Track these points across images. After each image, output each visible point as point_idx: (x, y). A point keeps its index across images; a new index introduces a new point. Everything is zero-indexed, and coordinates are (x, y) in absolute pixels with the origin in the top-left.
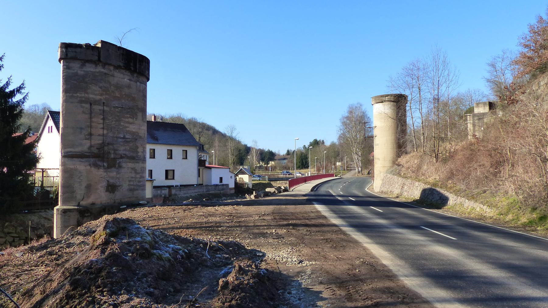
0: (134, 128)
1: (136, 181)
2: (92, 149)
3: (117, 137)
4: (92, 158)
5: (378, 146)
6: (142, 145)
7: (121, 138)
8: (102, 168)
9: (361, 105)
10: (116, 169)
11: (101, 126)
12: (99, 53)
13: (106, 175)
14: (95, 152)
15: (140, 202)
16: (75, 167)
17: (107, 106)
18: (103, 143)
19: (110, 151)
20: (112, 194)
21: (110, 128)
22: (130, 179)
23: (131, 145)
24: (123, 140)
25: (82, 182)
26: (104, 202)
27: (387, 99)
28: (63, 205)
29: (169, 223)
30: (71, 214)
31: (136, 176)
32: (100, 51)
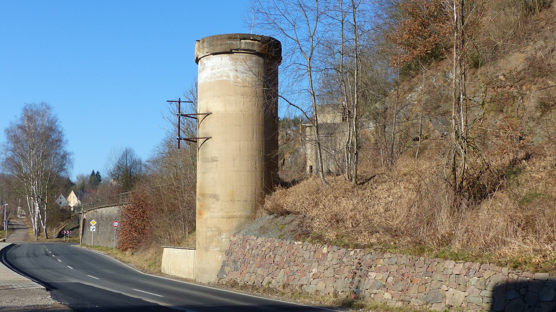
5: (215, 162)
9: (48, 108)
27: (243, 46)
29: (276, 21)
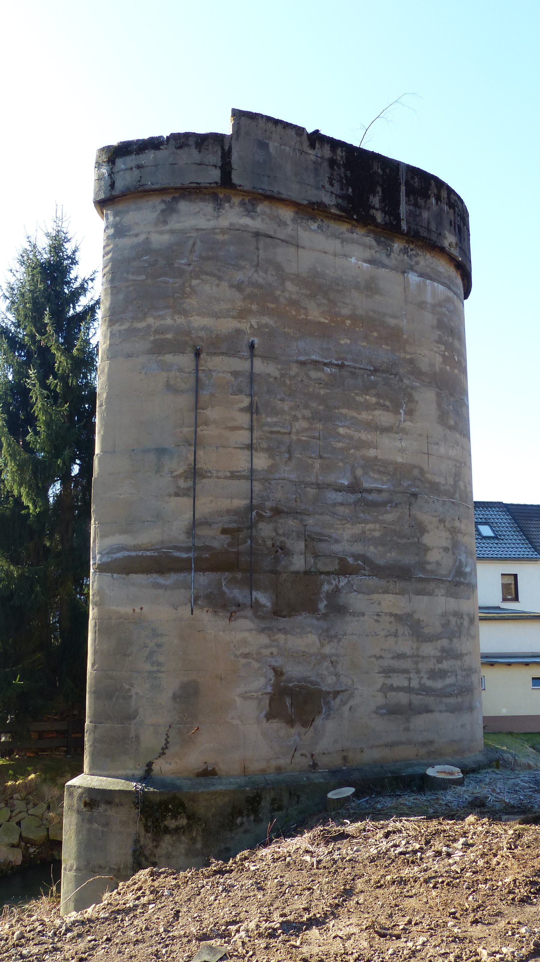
0: (402, 450)
1: (418, 672)
2: (203, 531)
3: (319, 486)
4: (197, 570)
6: (442, 521)
7: (339, 489)
8: (249, 612)
10: (318, 619)
11: (243, 437)
12: (226, 155)
13: (267, 647)
14: (216, 544)
15: (431, 772)
16: (138, 610)
17: (265, 358)
18: (251, 508)
19: (289, 543)
20: (298, 728)
21: (283, 449)
22: (387, 662)
23: (390, 517)
24: (352, 498)
25: (159, 675)
26: (262, 765)
28: (94, 772)
30: (112, 812)
31: (418, 649)
32: (230, 148)
